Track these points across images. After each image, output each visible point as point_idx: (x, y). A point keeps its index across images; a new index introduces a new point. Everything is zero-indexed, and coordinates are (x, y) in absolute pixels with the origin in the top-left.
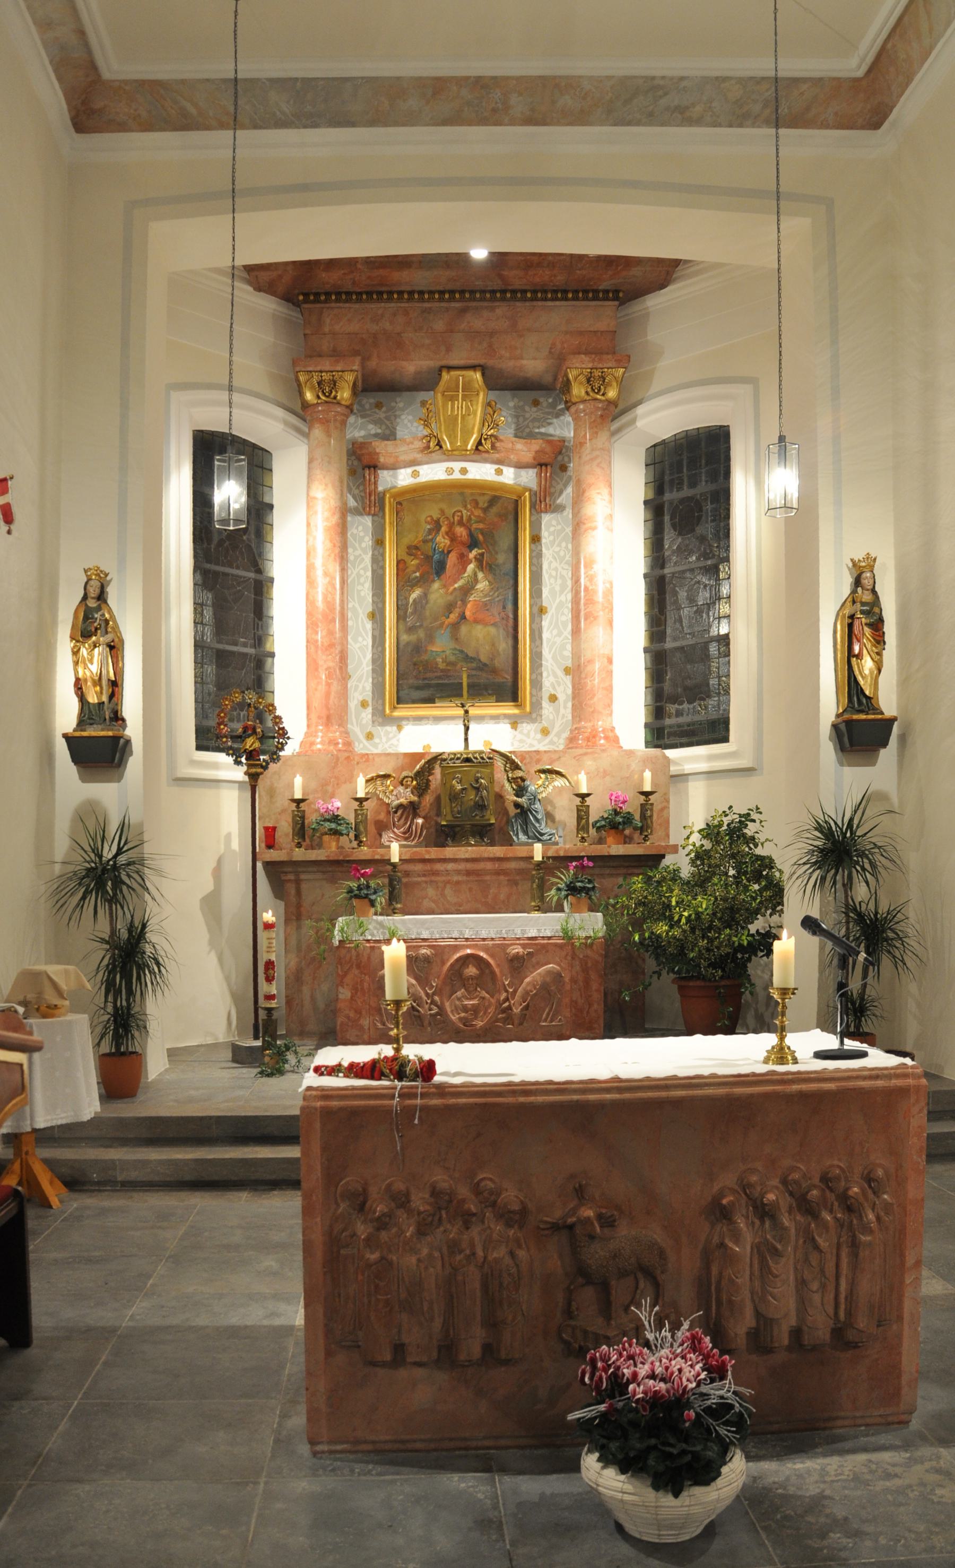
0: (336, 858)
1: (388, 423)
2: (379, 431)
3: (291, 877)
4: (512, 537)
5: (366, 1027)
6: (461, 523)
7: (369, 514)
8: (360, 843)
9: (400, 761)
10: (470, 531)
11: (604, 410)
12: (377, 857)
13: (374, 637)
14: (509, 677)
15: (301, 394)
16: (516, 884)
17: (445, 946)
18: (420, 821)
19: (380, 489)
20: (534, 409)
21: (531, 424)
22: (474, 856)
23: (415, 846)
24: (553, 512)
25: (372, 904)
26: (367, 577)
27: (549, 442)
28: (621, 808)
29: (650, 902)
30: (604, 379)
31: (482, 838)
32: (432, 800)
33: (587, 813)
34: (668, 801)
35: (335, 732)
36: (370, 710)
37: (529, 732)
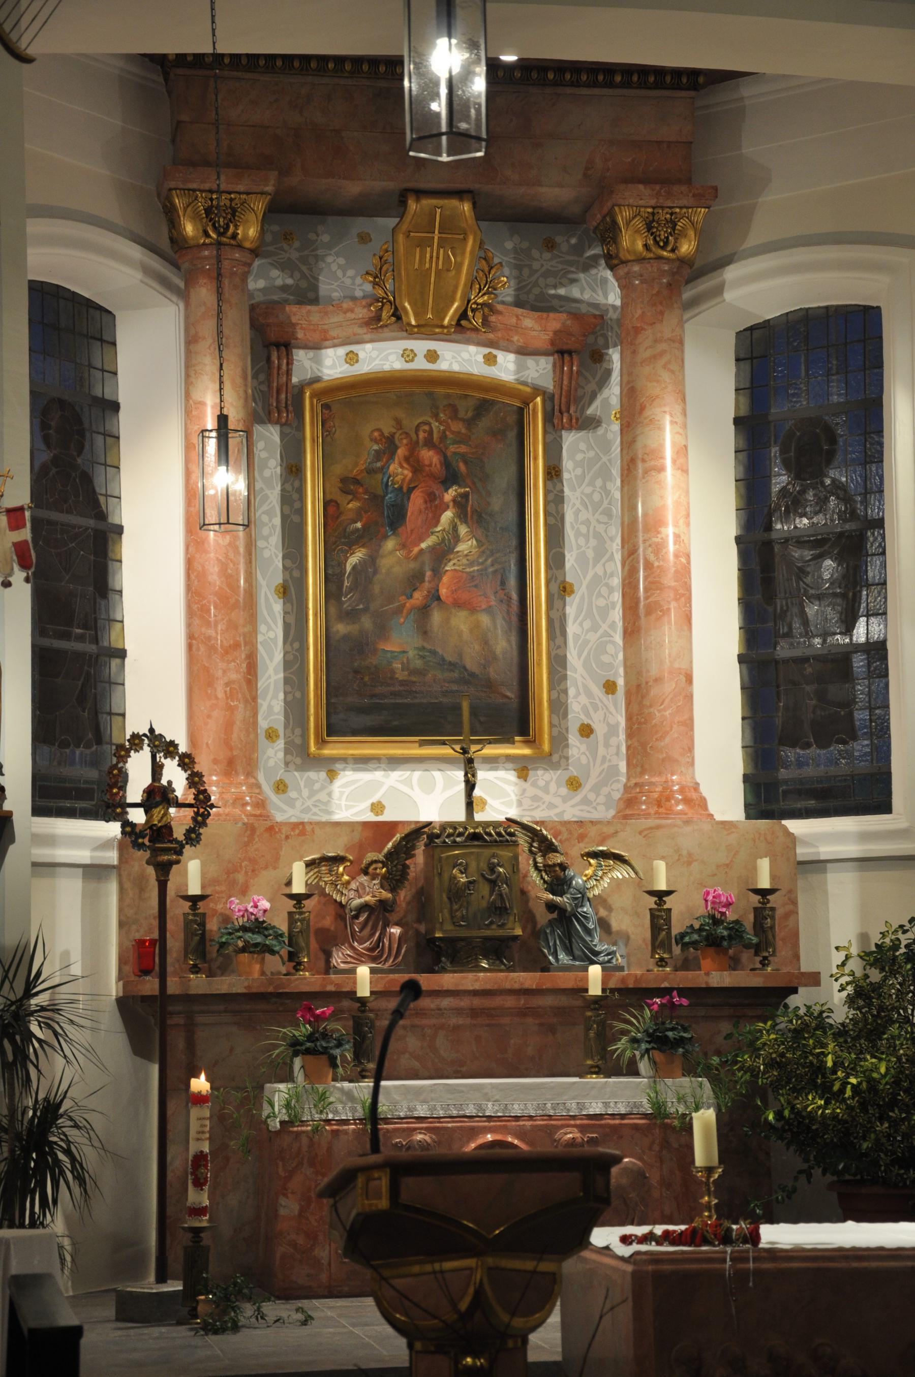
0: (262, 990)
1: (304, 268)
2: (290, 281)
3: (181, 1020)
4: (513, 469)
5: (325, 1262)
6: (429, 443)
7: (277, 422)
8: (298, 966)
9: (357, 836)
10: (445, 457)
11: (674, 274)
12: (330, 988)
13: (286, 626)
14: (511, 694)
15: (173, 223)
16: (552, 1030)
17: (453, 1129)
18: (396, 931)
19: (295, 380)
20: (547, 255)
21: (541, 281)
22: (488, 987)
23: (390, 971)
24: (580, 428)
25: (333, 1064)
26: (274, 527)
27: (576, 316)
28: (723, 914)
29: (789, 1062)
30: (675, 225)
31: (499, 959)
32: (409, 898)
33: (668, 921)
34: (794, 903)
35: (241, 784)
36: (280, 744)
37: (548, 783)
